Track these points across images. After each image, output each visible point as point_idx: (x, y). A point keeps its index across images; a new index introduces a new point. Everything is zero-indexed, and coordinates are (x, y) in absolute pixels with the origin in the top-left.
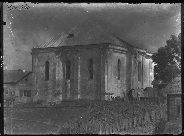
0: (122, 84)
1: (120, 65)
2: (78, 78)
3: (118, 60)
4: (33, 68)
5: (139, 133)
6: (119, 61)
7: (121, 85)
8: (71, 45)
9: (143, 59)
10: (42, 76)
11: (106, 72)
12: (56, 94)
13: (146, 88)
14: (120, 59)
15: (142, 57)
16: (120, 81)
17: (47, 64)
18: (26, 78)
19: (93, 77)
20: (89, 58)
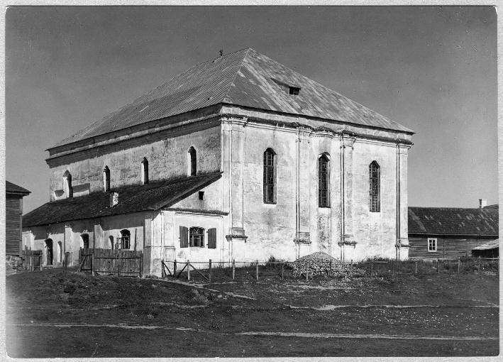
6: (375, 165)
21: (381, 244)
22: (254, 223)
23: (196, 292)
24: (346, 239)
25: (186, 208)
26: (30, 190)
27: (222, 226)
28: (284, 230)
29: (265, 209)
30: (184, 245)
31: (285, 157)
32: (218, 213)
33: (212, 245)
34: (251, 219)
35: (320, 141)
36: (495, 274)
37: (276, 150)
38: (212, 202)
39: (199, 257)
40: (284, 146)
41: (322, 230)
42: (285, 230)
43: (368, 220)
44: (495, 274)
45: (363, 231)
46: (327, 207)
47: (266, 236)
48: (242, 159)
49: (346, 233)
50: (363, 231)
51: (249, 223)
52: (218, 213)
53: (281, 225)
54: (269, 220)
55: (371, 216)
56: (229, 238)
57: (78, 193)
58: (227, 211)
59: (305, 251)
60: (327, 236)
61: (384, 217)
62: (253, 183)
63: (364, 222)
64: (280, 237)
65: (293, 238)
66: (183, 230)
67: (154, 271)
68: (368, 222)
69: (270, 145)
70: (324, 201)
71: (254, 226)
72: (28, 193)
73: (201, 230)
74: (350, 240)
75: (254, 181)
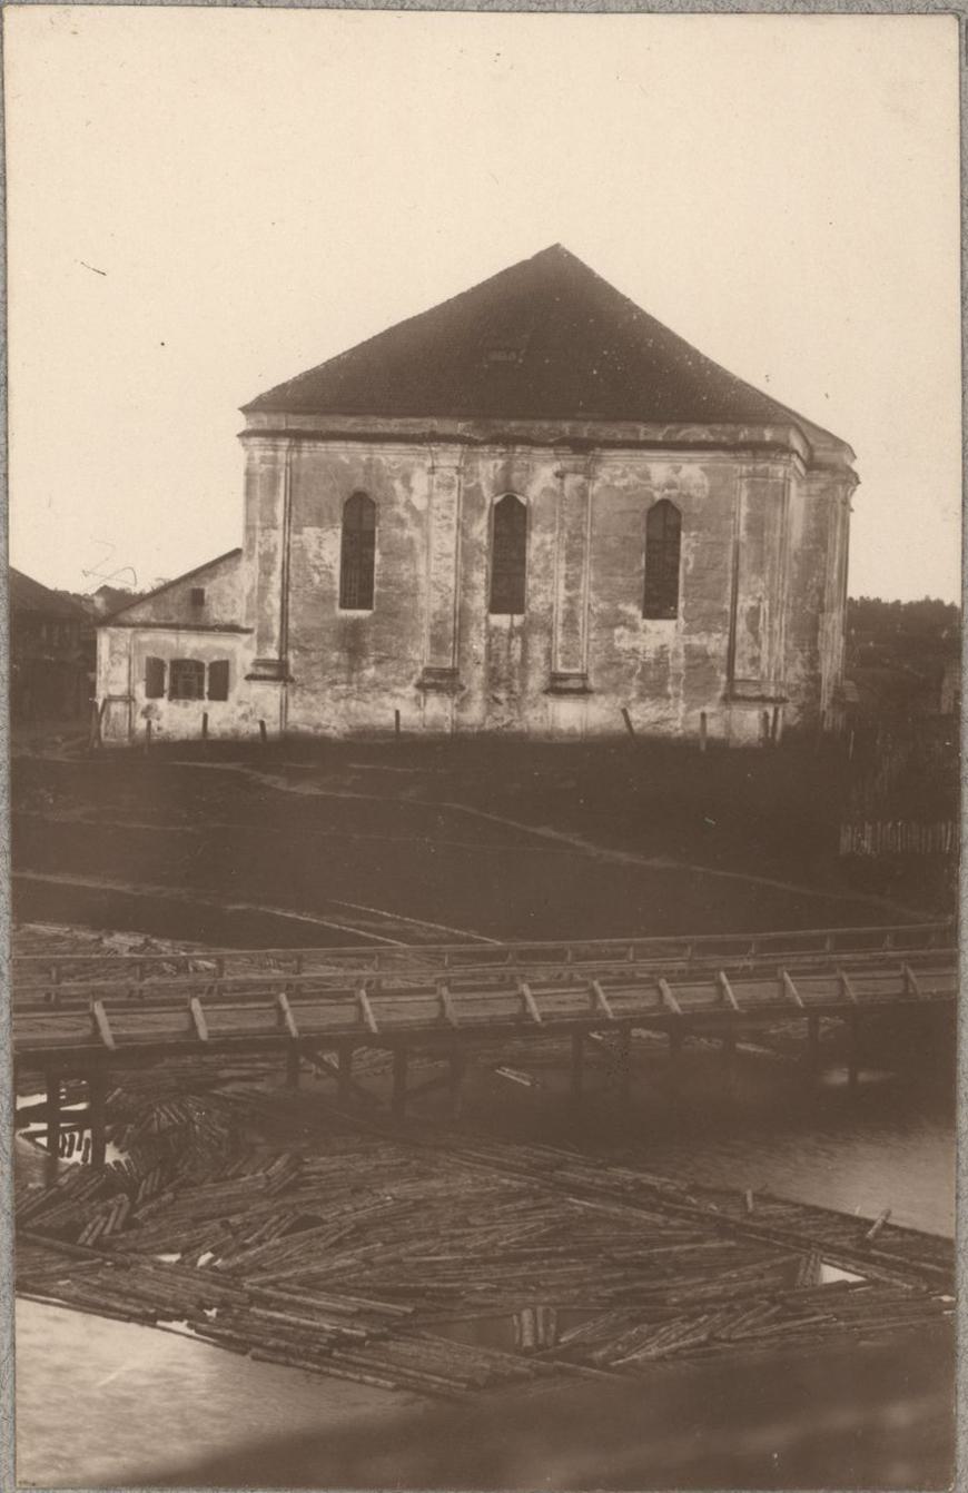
21: (677, 695)
22: (314, 650)
24: (559, 684)
25: (162, 621)
26: (240, 412)
27: (243, 653)
28: (391, 665)
29: (344, 621)
30: (154, 691)
32: (233, 629)
33: (220, 693)
35: (495, 466)
37: (377, 494)
38: (220, 609)
39: (178, 718)
40: (398, 485)
41: (492, 664)
43: (635, 638)
47: (343, 676)
51: (303, 650)
52: (233, 629)
53: (383, 654)
54: (353, 642)
56: (250, 677)
57: (88, 885)
58: (250, 626)
59: (438, 709)
60: (505, 675)
61: (688, 631)
62: (315, 567)
64: (381, 677)
65: (414, 681)
66: (155, 668)
68: (637, 643)
69: (359, 484)
72: (241, 409)
73: (199, 666)
75: (317, 563)
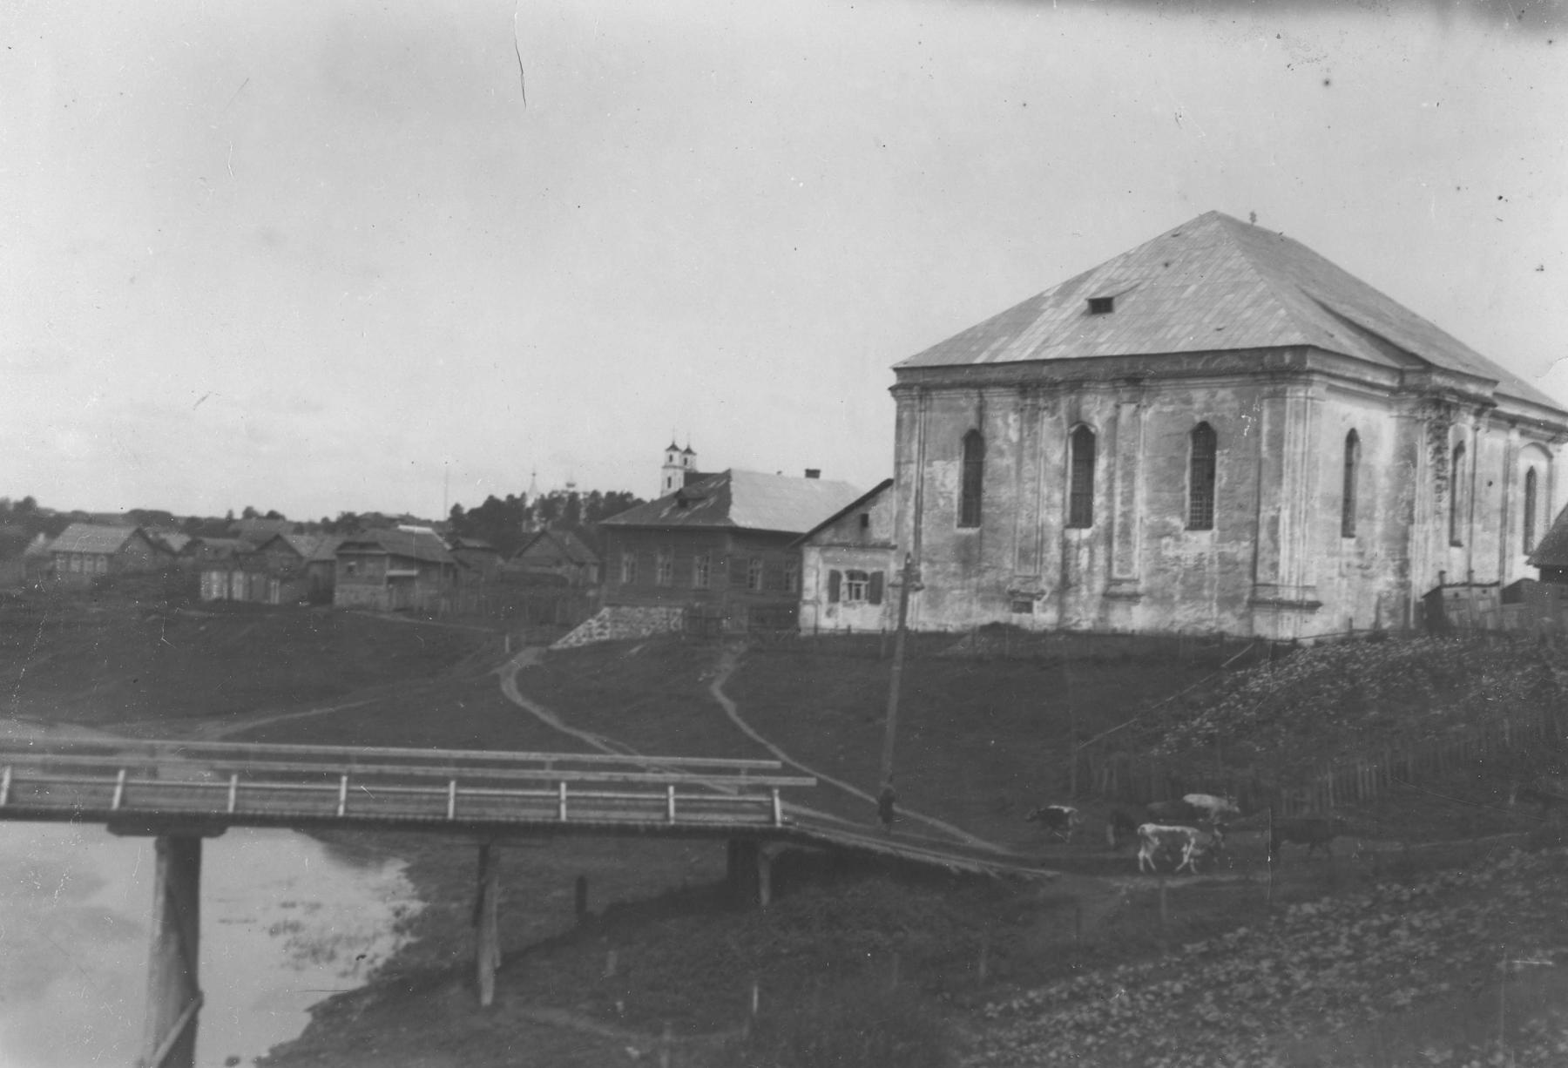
0: (1361, 555)
1: (1359, 455)
2: (1134, 521)
3: (1347, 430)
4: (898, 464)
5: (647, 615)
6: (1352, 438)
7: (1356, 561)
8: (1102, 351)
9: (1477, 429)
10: (941, 502)
11: (640, 759)
12: (1166, 525)
13: (1519, 584)
14: (1359, 427)
15: (1471, 420)
16: (1353, 541)
17: (974, 445)
18: (861, 510)
19: (1216, 516)
20: (1198, 419)
23: (1472, 702)
31: (999, 442)
32: (885, 546)
34: (935, 554)
36: (769, 799)
42: (995, 571)
43: (1178, 547)
44: (769, 799)
45: (1165, 571)
46: (727, 486)
48: (915, 457)
49: (1116, 575)
50: (1165, 571)
52: (885, 546)
55: (1187, 540)
61: (1222, 540)
63: (1170, 553)
67: (343, 591)
68: (1180, 552)
70: (1080, 514)
71: (938, 567)
74: (1126, 588)
75: (942, 489)
